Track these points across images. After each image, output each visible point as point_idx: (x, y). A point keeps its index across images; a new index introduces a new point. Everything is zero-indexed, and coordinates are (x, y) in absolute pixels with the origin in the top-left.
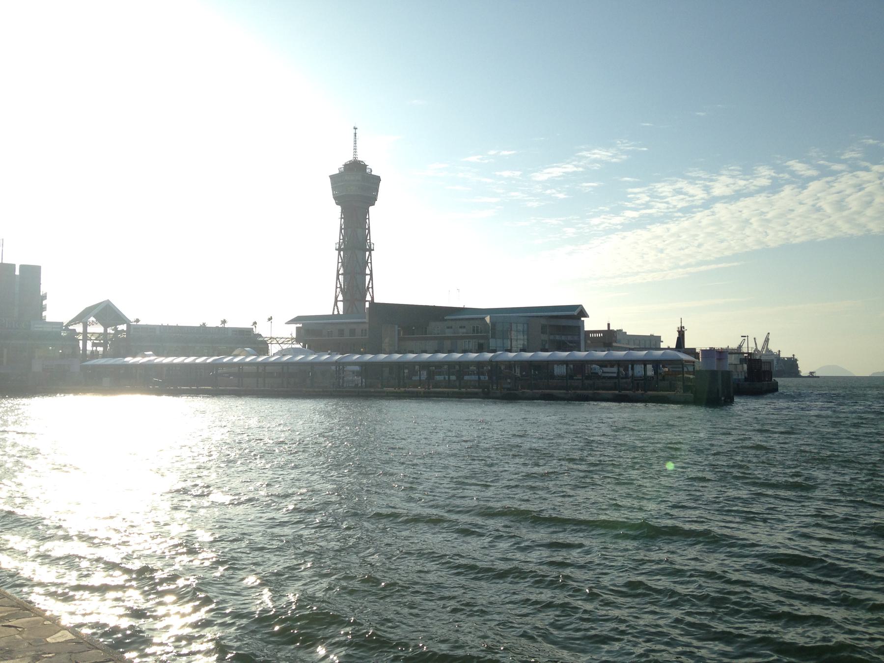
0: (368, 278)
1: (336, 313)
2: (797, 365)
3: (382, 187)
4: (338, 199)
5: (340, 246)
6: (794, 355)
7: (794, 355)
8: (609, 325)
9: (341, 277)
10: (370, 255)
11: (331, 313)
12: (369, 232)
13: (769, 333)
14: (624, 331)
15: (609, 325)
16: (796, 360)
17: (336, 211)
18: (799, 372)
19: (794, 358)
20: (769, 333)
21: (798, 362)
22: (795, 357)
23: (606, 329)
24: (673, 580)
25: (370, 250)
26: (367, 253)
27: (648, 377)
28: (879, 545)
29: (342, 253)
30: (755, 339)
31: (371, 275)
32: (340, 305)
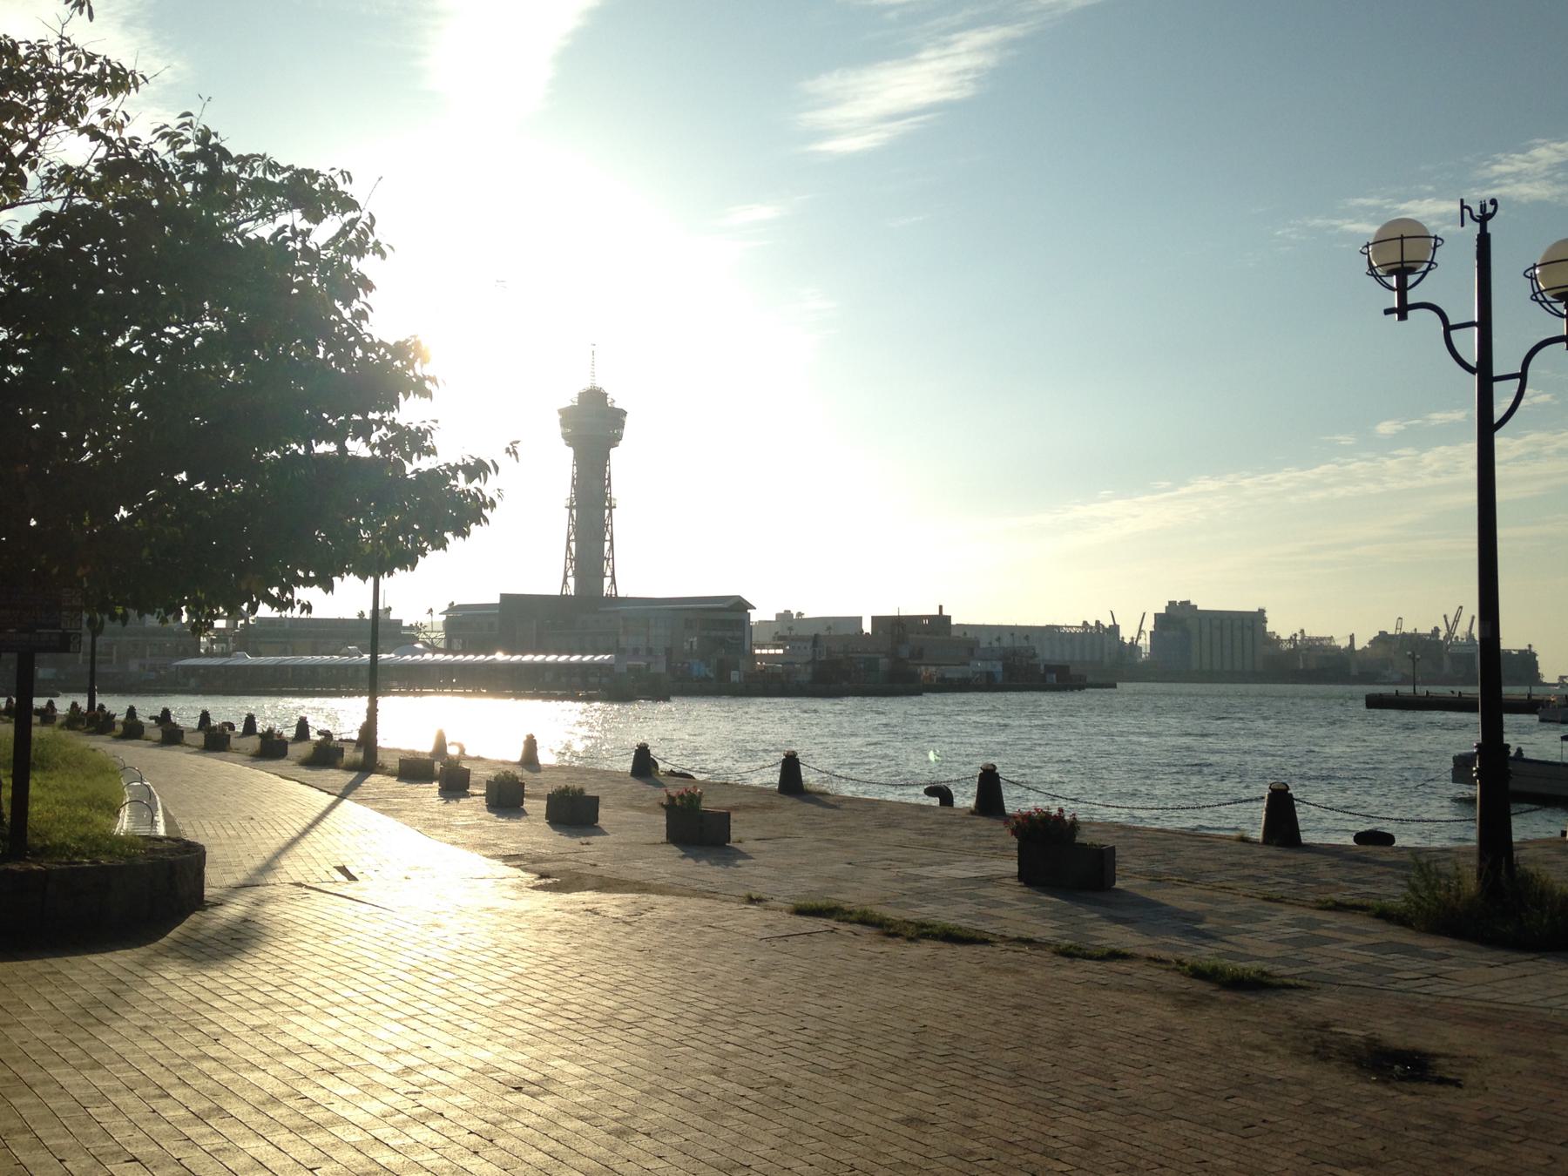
0: (607, 545)
1: (564, 593)
2: (1536, 663)
3: (628, 420)
4: (570, 440)
5: (571, 502)
6: (1530, 646)
7: (1530, 646)
8: (941, 607)
9: (573, 545)
10: (610, 514)
11: (559, 594)
12: (609, 485)
13: (1461, 607)
14: (1193, 603)
15: (941, 607)
16: (1535, 655)
17: (569, 453)
18: (1538, 676)
19: (1530, 650)
20: (1461, 607)
21: (1537, 658)
22: (1533, 649)
23: (937, 613)
24: (1312, 968)
25: (611, 508)
26: (607, 512)
27: (215, 728)
28: (1564, 973)
29: (574, 512)
30: (1445, 616)
31: (611, 541)
32: (571, 581)
